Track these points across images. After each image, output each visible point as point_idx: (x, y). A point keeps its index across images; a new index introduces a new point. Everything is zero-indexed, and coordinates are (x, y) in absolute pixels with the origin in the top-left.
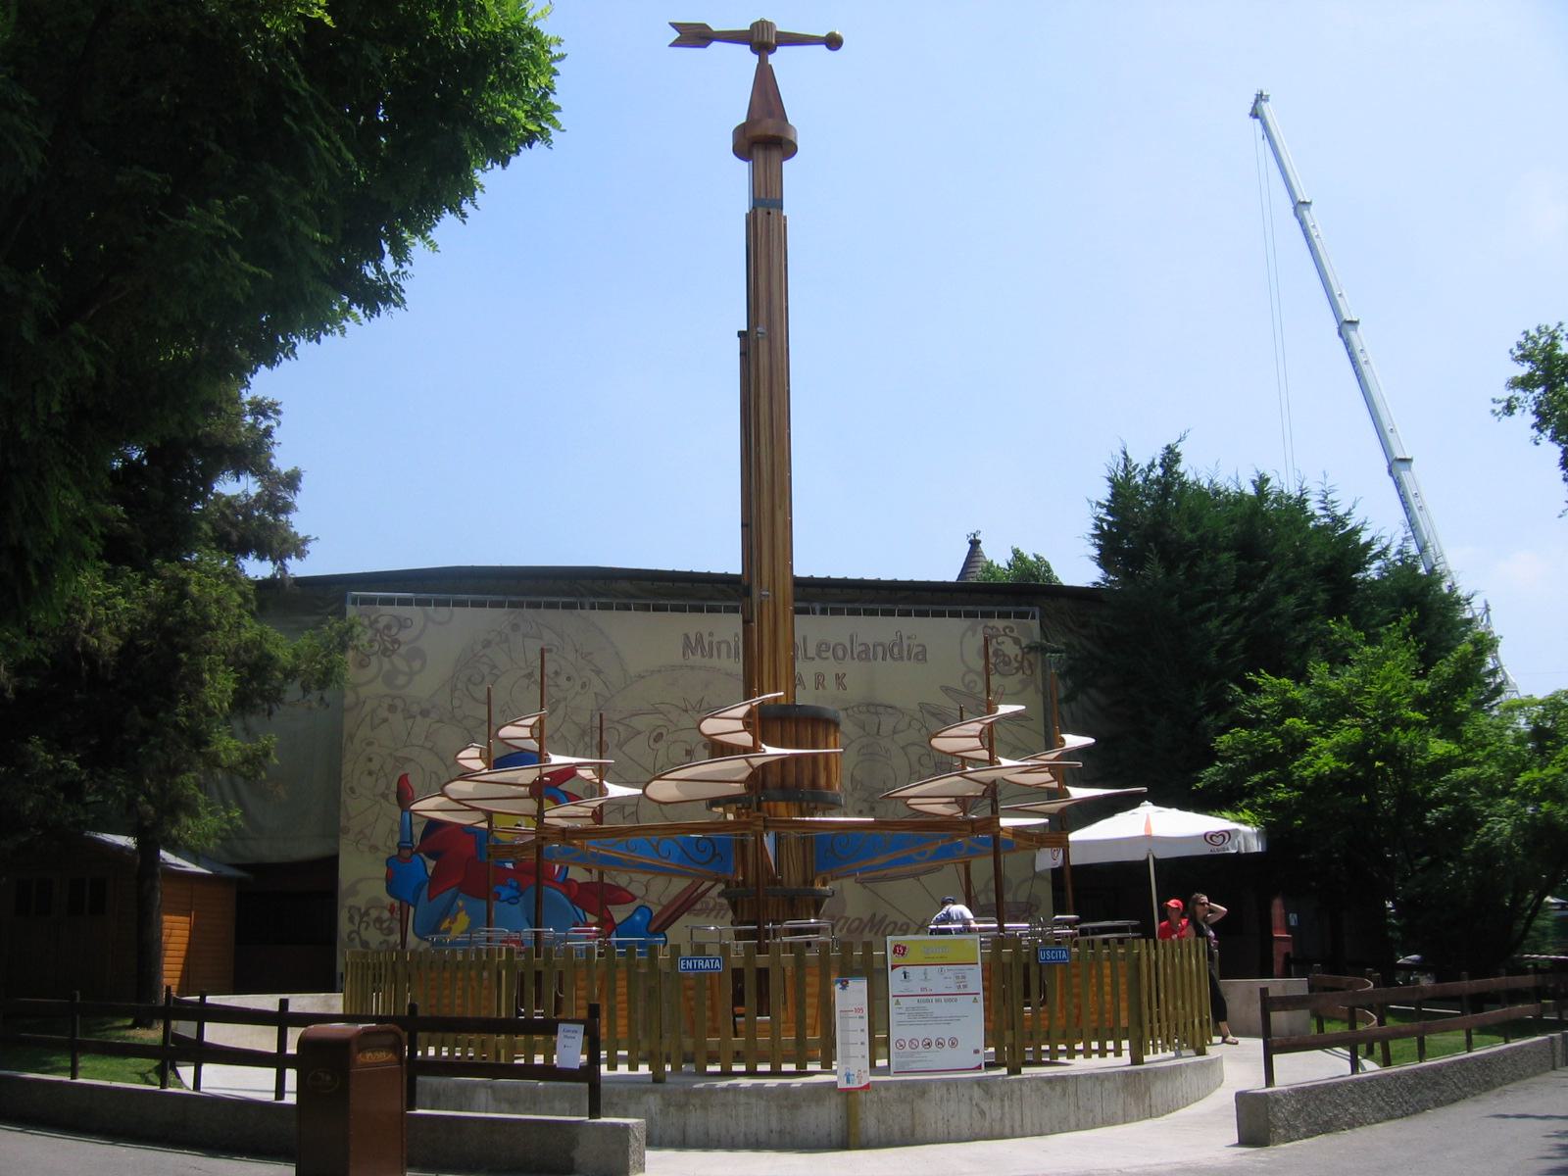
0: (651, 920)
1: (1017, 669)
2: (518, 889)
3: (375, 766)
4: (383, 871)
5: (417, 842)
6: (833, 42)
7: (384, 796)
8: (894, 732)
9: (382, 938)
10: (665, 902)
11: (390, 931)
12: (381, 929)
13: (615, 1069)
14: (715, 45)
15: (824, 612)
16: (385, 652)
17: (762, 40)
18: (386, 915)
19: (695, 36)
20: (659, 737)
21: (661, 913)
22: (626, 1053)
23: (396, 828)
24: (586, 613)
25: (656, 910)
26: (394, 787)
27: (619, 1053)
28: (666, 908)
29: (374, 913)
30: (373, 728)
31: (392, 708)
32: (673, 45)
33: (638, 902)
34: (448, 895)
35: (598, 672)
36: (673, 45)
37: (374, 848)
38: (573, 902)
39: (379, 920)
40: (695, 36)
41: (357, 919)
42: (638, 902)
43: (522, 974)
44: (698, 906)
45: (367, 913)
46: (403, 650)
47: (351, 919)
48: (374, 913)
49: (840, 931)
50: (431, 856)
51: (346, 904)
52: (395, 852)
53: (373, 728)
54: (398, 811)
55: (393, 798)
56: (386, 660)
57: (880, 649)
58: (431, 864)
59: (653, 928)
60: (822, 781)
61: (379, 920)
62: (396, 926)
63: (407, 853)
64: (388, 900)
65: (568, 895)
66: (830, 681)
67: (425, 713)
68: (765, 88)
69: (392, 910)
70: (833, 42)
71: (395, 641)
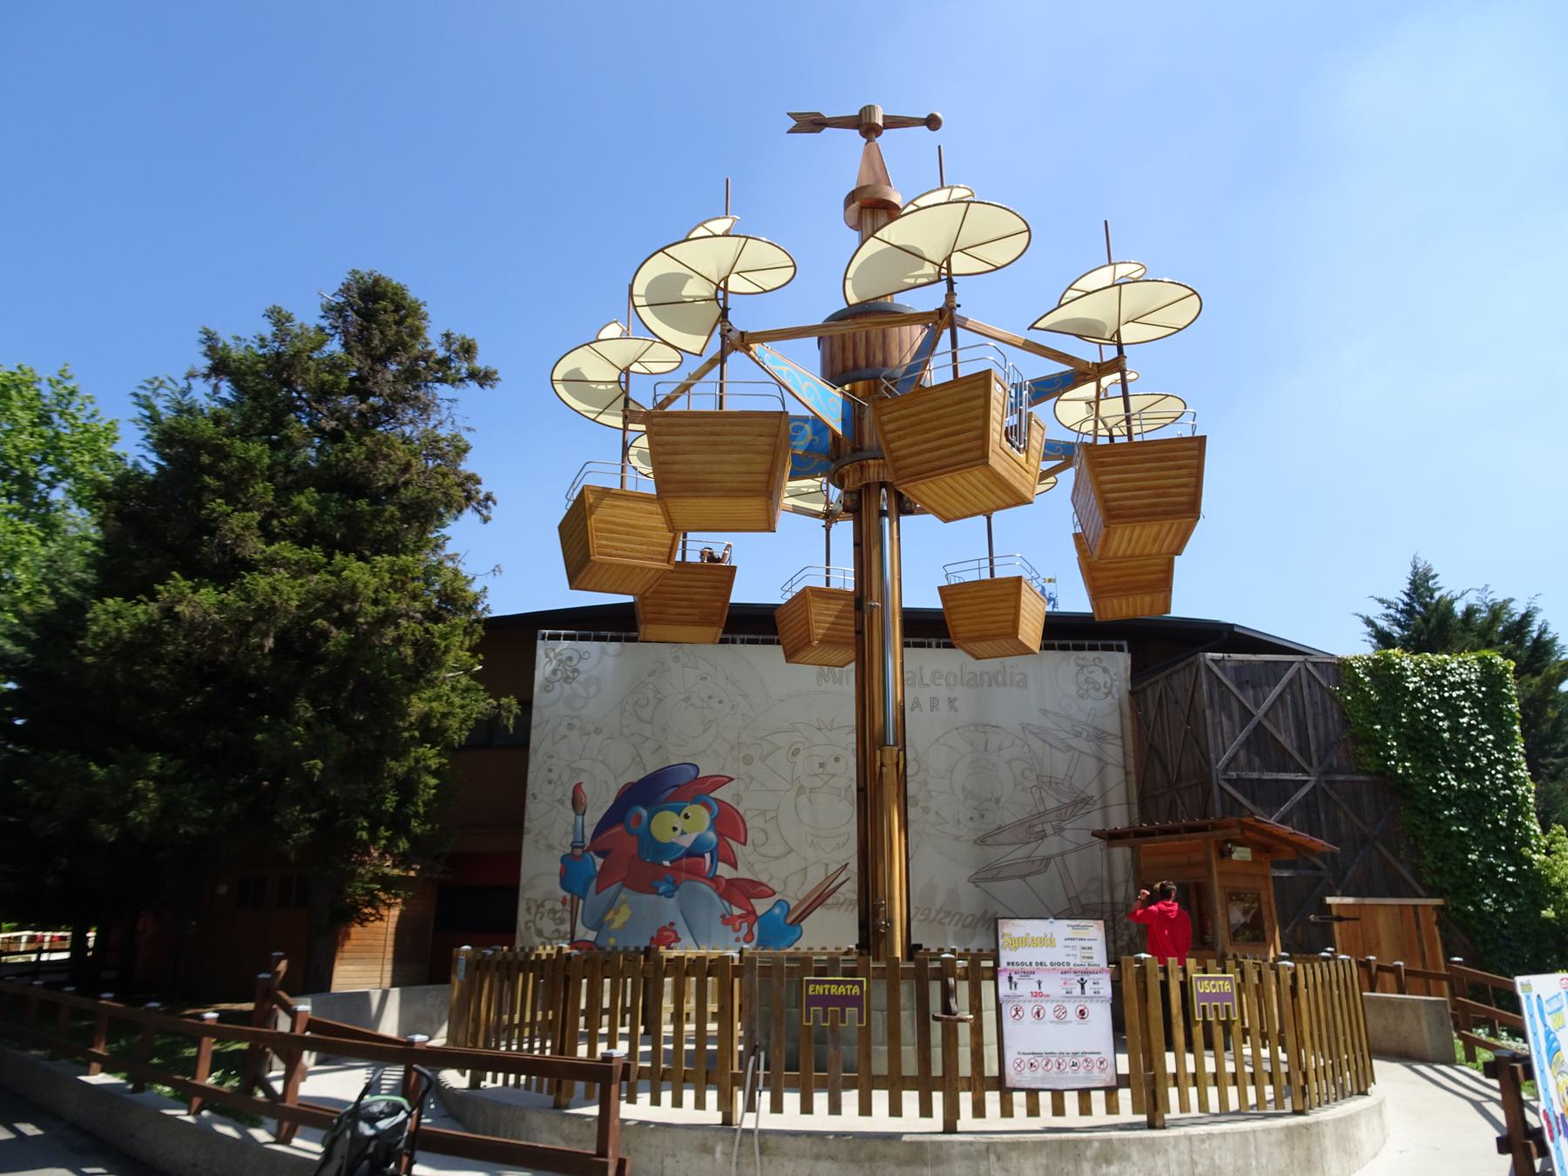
0: (789, 912)
1: (1107, 695)
2: (674, 883)
3: (553, 776)
4: (558, 866)
5: (587, 842)
6: (932, 122)
7: (561, 802)
8: (1000, 749)
9: (554, 927)
10: (801, 897)
11: (562, 921)
12: (554, 919)
13: (286, 1141)
14: (827, 129)
15: (938, 646)
16: (566, 679)
17: (865, 125)
18: (559, 906)
19: (811, 123)
20: (796, 753)
21: (797, 907)
22: (709, 1047)
23: (570, 829)
24: (739, 647)
25: (793, 904)
26: (570, 795)
27: (693, 1047)
28: (802, 902)
29: (548, 905)
30: (554, 743)
31: (571, 727)
32: (791, 131)
33: (777, 897)
34: (614, 888)
35: (745, 696)
36: (791, 131)
37: (551, 847)
38: (721, 896)
39: (553, 911)
40: (811, 123)
41: (533, 911)
42: (777, 897)
43: (1227, 1048)
44: (830, 901)
45: (542, 905)
46: (581, 678)
47: (528, 910)
48: (548, 905)
49: (887, 388)
50: (600, 854)
51: (527, 894)
52: (569, 851)
53: (554, 743)
54: (572, 814)
55: (569, 803)
56: (567, 686)
57: (986, 677)
58: (599, 861)
59: (790, 920)
60: (879, 357)
61: (553, 911)
62: (567, 916)
63: (579, 852)
64: (562, 893)
65: (716, 890)
66: (943, 704)
67: (598, 731)
68: (874, 162)
69: (564, 902)
70: (932, 122)
71: (576, 671)
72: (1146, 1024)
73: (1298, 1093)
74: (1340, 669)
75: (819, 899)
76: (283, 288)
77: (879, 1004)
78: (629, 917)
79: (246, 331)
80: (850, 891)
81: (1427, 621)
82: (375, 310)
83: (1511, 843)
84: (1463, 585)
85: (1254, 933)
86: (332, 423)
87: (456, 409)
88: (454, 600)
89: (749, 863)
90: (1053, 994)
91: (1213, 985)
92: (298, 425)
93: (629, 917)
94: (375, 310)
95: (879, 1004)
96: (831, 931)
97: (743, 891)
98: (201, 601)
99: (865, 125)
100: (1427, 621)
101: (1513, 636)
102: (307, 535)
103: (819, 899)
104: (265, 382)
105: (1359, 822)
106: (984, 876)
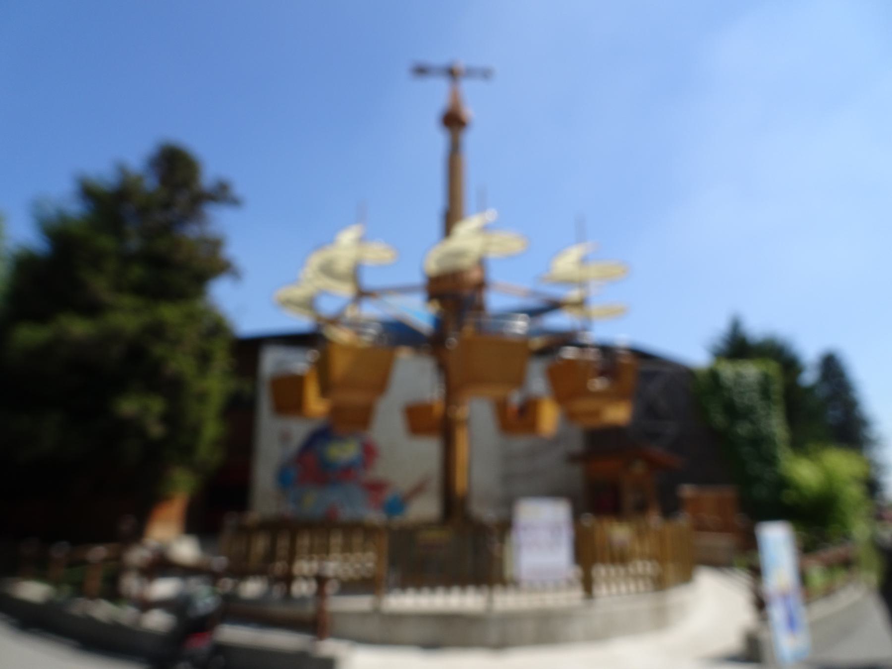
17: (452, 73)
19: (421, 71)
40: (421, 71)
72: (588, 554)
73: (660, 584)
74: (681, 374)
75: (418, 490)
76: (120, 151)
77: (468, 549)
78: (314, 501)
79: (102, 169)
80: (435, 484)
81: (738, 347)
82: (174, 164)
83: (771, 461)
84: (757, 327)
85: (642, 508)
86: (145, 233)
87: (220, 220)
88: (217, 328)
89: (380, 471)
90: (542, 537)
91: (620, 533)
92: (131, 228)
93: (314, 501)
94: (174, 164)
95: (468, 549)
96: (426, 508)
97: (376, 488)
98: (79, 328)
99: (452, 73)
100: (738, 347)
101: (779, 355)
102: (140, 290)
103: (418, 490)
104: (109, 205)
105: (703, 452)
106: (507, 478)
